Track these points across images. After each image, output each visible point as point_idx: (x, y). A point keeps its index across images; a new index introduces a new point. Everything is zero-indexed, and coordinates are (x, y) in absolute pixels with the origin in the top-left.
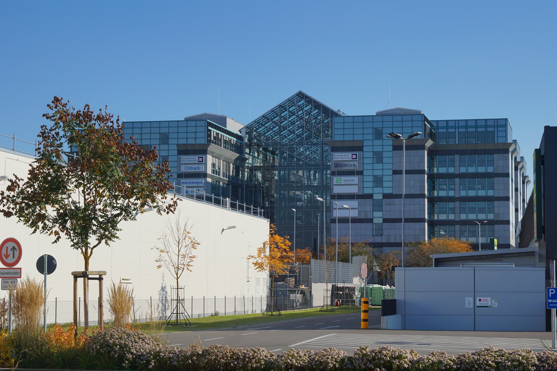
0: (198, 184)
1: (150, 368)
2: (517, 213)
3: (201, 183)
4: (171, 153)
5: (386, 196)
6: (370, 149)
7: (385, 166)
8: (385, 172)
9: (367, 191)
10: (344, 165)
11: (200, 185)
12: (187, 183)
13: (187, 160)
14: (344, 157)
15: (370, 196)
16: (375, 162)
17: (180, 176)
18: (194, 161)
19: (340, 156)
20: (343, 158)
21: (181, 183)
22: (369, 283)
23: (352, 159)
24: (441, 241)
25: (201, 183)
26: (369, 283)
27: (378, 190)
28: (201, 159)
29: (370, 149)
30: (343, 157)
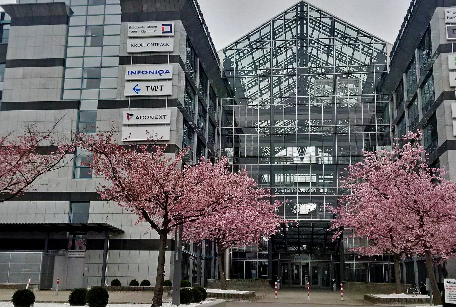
0: (160, 74)
1: (90, 290)
2: (237, 144)
3: (168, 72)
4: (109, 20)
5: (103, 104)
6: (82, 20)
7: (107, 51)
8: (106, 62)
9: (68, 96)
10: (134, 45)
11: (164, 76)
12: (138, 72)
13: (139, 30)
14: (148, 29)
15: (76, 105)
16: (89, 43)
17: (62, 62)
18: (155, 31)
19: (139, 27)
20: (145, 32)
21: (127, 73)
22: (417, 261)
23: (163, 33)
24: (433, 202)
25: (168, 72)
26: (417, 261)
27: (93, 94)
28: (167, 29)
29: (82, 20)
30: (145, 29)
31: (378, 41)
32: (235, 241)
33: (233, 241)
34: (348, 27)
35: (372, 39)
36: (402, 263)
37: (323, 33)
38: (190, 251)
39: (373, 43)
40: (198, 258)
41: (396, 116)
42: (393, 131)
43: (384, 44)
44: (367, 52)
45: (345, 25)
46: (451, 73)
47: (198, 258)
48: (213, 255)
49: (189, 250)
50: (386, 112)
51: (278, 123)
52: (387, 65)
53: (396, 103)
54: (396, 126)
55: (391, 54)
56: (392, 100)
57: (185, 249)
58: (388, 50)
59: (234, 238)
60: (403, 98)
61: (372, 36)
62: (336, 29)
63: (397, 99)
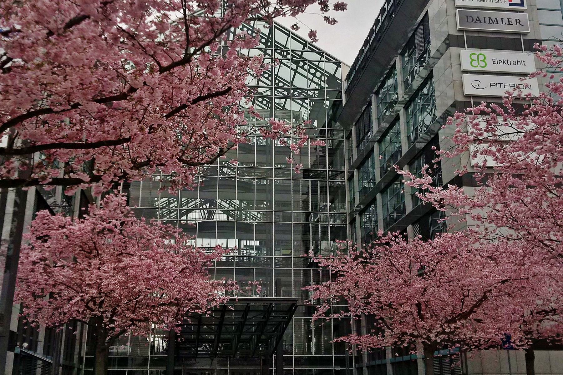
31: (330, 59)
32: (136, 320)
33: (132, 320)
34: (292, 37)
35: (322, 56)
36: (362, 368)
37: (257, 104)
38: (38, 351)
39: (323, 62)
40: (54, 365)
41: (355, 157)
42: (351, 178)
43: (338, 64)
44: (317, 71)
45: (288, 35)
46: (465, 76)
47: (54, 365)
48: (75, 361)
49: (35, 351)
50: (338, 155)
51: (226, 202)
52: (341, 92)
53: (357, 139)
54: (355, 173)
55: (349, 76)
56: (349, 137)
57: (29, 348)
58: (342, 74)
59: (136, 315)
60: (370, 129)
61: (323, 53)
62: (275, 41)
63: (358, 134)
